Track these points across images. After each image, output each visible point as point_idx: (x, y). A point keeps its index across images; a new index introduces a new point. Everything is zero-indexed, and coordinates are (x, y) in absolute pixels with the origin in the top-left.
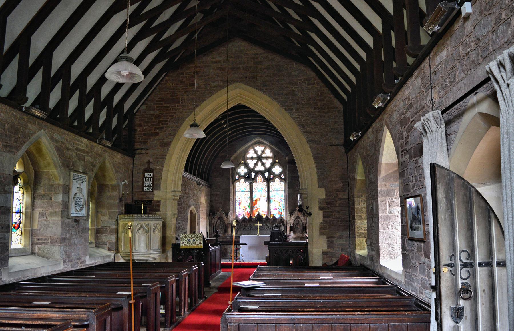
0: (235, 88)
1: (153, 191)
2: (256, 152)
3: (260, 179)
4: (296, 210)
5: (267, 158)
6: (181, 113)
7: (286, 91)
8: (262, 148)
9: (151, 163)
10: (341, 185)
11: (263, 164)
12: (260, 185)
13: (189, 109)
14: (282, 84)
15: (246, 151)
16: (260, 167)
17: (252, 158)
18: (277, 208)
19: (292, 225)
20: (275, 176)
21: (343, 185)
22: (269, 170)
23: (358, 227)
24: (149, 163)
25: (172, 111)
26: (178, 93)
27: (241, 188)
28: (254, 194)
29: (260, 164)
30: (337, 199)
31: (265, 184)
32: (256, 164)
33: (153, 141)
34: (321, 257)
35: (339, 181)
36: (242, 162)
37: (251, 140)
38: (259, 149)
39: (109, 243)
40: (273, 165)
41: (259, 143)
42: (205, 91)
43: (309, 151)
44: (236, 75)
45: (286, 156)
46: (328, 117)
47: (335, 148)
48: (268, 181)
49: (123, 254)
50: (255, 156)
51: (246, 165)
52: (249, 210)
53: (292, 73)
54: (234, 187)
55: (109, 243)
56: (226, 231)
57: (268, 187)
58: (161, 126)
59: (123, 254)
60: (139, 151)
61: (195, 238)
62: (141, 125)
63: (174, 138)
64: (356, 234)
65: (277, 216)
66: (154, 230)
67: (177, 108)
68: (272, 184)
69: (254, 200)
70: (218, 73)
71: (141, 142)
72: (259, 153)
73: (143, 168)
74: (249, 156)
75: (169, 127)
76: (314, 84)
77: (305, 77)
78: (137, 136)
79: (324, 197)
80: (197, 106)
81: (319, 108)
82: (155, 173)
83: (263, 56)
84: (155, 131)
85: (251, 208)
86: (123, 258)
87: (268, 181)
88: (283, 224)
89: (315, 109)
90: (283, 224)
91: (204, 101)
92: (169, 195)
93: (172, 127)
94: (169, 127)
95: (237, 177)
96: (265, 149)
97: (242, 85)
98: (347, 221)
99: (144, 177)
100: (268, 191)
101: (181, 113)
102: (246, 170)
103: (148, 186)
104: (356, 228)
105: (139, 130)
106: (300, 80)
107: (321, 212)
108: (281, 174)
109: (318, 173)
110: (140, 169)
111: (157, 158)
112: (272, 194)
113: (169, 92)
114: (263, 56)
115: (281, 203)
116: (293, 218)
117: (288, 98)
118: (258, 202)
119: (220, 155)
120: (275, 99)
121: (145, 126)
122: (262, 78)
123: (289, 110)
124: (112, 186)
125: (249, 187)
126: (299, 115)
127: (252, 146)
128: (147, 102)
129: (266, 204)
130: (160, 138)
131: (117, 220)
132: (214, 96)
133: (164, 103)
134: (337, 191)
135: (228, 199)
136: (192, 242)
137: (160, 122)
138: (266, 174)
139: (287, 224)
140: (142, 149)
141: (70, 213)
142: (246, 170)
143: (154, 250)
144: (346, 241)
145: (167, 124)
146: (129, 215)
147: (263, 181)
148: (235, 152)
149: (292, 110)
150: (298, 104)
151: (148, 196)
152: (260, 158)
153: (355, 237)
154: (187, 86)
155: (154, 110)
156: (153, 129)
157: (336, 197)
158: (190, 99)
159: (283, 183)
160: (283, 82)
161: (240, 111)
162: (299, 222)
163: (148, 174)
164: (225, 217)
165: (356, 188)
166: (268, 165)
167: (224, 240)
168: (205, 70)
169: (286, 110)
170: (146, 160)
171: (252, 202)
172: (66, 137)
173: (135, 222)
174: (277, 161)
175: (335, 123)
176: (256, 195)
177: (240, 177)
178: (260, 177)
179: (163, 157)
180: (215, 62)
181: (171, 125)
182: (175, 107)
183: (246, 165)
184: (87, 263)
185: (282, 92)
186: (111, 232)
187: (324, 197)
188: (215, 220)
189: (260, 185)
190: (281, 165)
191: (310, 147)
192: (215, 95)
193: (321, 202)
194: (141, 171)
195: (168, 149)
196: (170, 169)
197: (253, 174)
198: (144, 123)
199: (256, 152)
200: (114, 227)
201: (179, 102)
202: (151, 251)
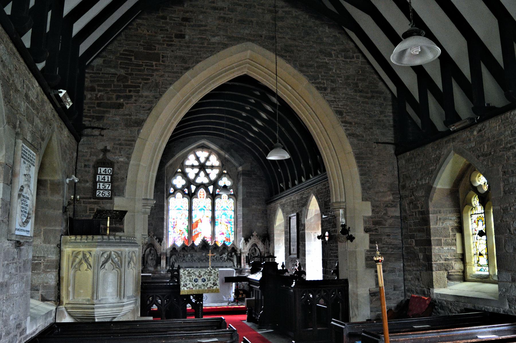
0: (246, 50)
1: (111, 198)
2: (198, 159)
3: (202, 194)
4: (253, 235)
5: (212, 167)
6: (162, 76)
7: (317, 62)
9: (109, 151)
10: (391, 198)
11: (207, 175)
12: (202, 201)
13: (174, 73)
14: (311, 52)
15: (185, 157)
16: (202, 179)
17: (193, 167)
18: (224, 232)
19: (247, 255)
21: (394, 198)
23: (435, 255)
24: (105, 151)
25: (146, 72)
26: (157, 46)
28: (194, 213)
29: (202, 174)
30: (386, 217)
31: (209, 201)
32: (197, 175)
33: (113, 116)
34: (369, 300)
35: (389, 193)
36: (179, 170)
37: (195, 141)
38: (202, 155)
39: (44, 287)
40: (220, 176)
41: (203, 147)
42: (201, 47)
43: (349, 148)
44: (247, 32)
45: (240, 165)
46: (372, 104)
47: (381, 146)
48: (213, 197)
49: (72, 308)
50: (196, 163)
51: (184, 175)
52: (186, 235)
53: (325, 39)
54: (168, 203)
55: (44, 287)
56: (158, 262)
57: (213, 205)
58: (128, 94)
59: (72, 308)
60: (89, 130)
61: (205, 277)
62: (93, 89)
63: (149, 114)
64: (434, 266)
66: (129, 263)
67: (155, 67)
68: (217, 201)
70: (219, 25)
71: (92, 117)
72: (202, 160)
73: (94, 158)
74: (187, 163)
75: (142, 96)
76: (353, 57)
77: (342, 47)
78: (86, 107)
79: (370, 214)
80: (187, 69)
81: (361, 91)
82: (116, 168)
83: (284, 9)
84: (118, 101)
85: (190, 232)
86: (70, 314)
87: (213, 197)
88: (236, 254)
89: (356, 91)
90: (236, 254)
91: (197, 62)
92: (139, 206)
93: (146, 97)
94: (142, 96)
95: (172, 190)
96: (209, 155)
97: (256, 47)
98: (399, 248)
99: (96, 174)
100: (213, 210)
101: (162, 76)
102: (183, 182)
103: (103, 189)
104: (433, 257)
105: (89, 96)
106: (335, 50)
107: (367, 235)
109: (361, 180)
110: (88, 160)
111: (120, 144)
112: (217, 214)
113: (141, 43)
114: (284, 9)
115: (229, 225)
116: (249, 246)
117: (321, 72)
118: (200, 224)
120: (301, 71)
121: (99, 91)
122: (283, 40)
123: (321, 89)
124: (53, 183)
125: (187, 205)
126: (335, 98)
127: (193, 151)
128: (104, 54)
129: (209, 227)
130: (126, 112)
131: (59, 246)
132: (212, 59)
133: (133, 58)
134: (387, 206)
135: (162, 220)
136: (200, 283)
137: (126, 87)
138: (211, 188)
139: (241, 254)
140: (93, 128)
141: (13, 229)
142: (183, 182)
143: (129, 298)
144: (399, 276)
145: (138, 92)
146: (84, 237)
147: (207, 197)
148: (173, 156)
149: (325, 89)
150: (332, 81)
151: (102, 206)
152: (202, 167)
153: (432, 270)
154: (172, 38)
155: (115, 67)
156: (114, 96)
157: (385, 214)
158: (176, 57)
159: (232, 201)
160: (313, 50)
161: (245, 84)
162: (256, 250)
163: (103, 169)
164: (157, 244)
165: (432, 200)
166: (213, 177)
167: (156, 275)
168: (201, 17)
169: (318, 88)
170: (100, 147)
171: (191, 225)
172: (15, 62)
173: (96, 250)
174: (225, 172)
175: (382, 113)
176: (197, 215)
177: (176, 190)
178: (202, 192)
179: (130, 143)
180: (215, 8)
181: (145, 94)
182: (152, 66)
183: (184, 175)
184: (28, 332)
185: (311, 63)
186: (47, 267)
187: (370, 214)
189: (202, 201)
191: (351, 144)
192: (215, 56)
193: (366, 220)
194: (92, 164)
195: (139, 131)
196: (141, 163)
197: (193, 188)
198: (98, 85)
199: (198, 159)
200: (53, 257)
201: (158, 60)
202: (125, 300)
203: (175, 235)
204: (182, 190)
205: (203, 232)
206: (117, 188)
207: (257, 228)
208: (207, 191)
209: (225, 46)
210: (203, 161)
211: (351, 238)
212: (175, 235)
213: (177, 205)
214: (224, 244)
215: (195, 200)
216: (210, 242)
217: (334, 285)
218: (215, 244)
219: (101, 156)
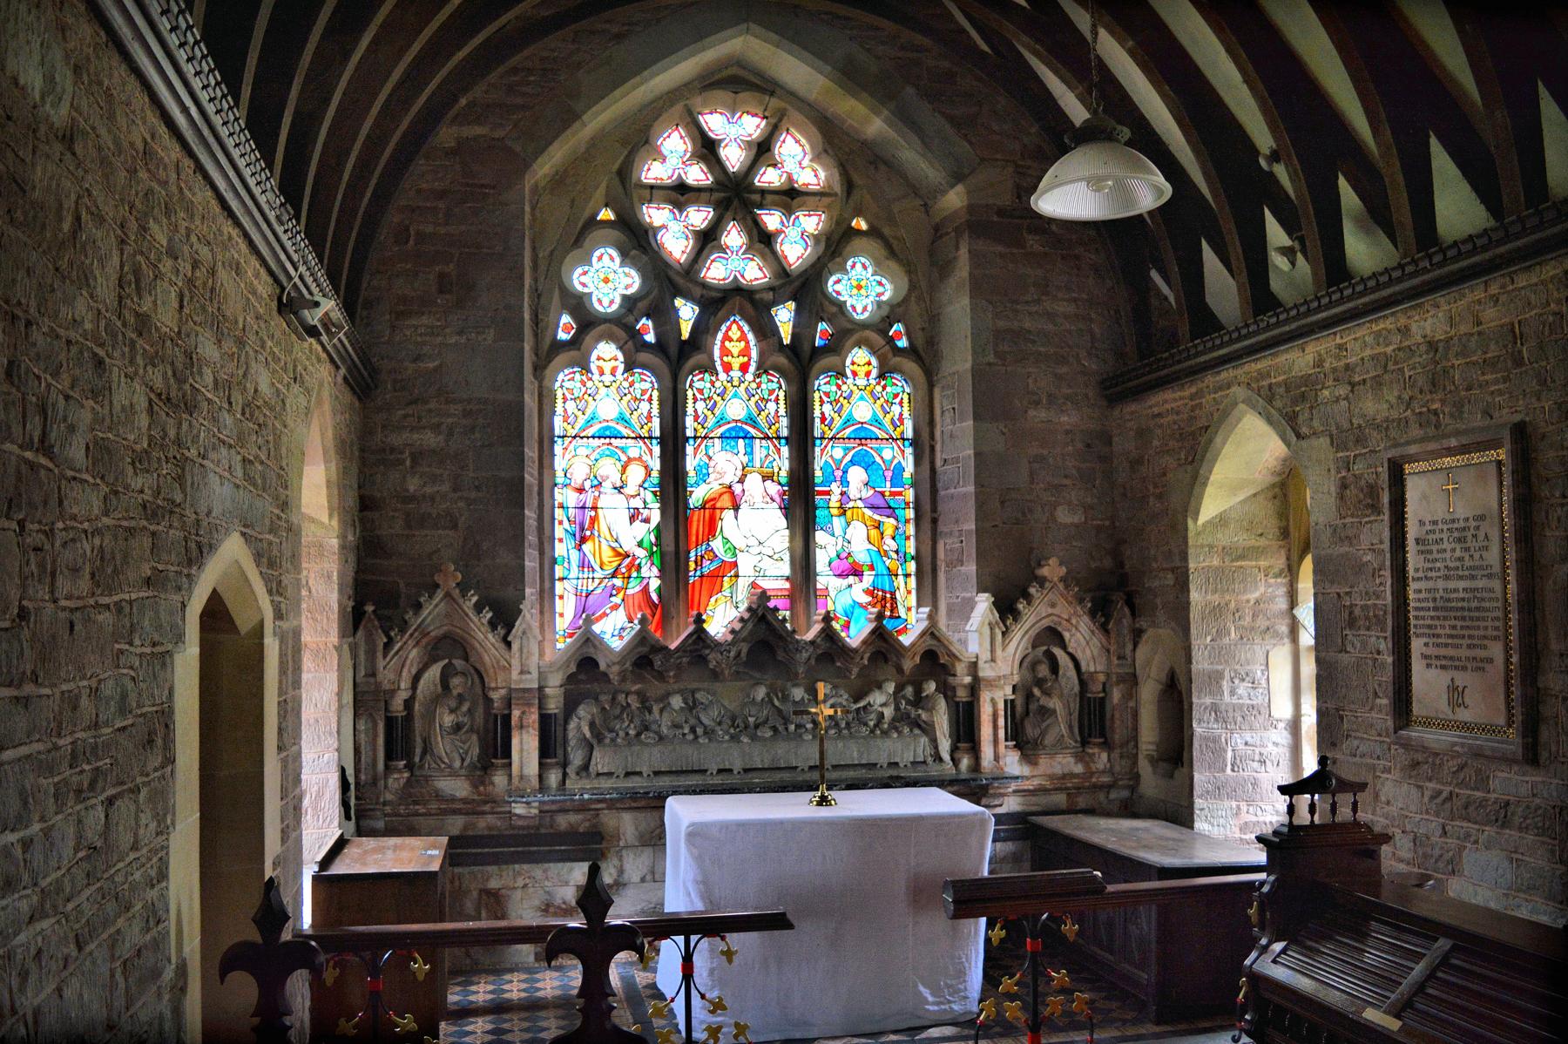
2: (707, 149)
8: (752, 126)
11: (763, 241)
15: (638, 138)
16: (735, 264)
20: (847, 332)
22: (806, 288)
27: (595, 424)
31: (774, 387)
32: (707, 240)
36: (606, 214)
40: (833, 247)
48: (799, 365)
51: (637, 242)
54: (546, 401)
56: (497, 748)
65: (857, 633)
69: (697, 496)
74: (655, 172)
87: (799, 365)
88: (946, 690)
90: (946, 690)
100: (801, 439)
108: (890, 314)
119: (446, 135)
127: (681, 106)
139: (974, 689)
148: (570, 118)
164: (485, 640)
171: (682, 522)
176: (713, 467)
177: (589, 323)
178: (735, 339)
183: (637, 242)
188: (405, 669)
189: (735, 392)
190: (891, 251)
197: (687, 312)
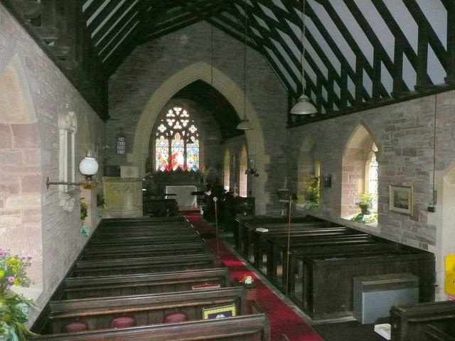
11: (181, 124)
12: (178, 141)
16: (178, 126)
40: (189, 125)
48: (184, 138)
51: (166, 124)
80: (166, 79)
102: (165, 128)
118: (176, 157)
138: (184, 133)
142: (165, 128)
152: (178, 118)
166: (185, 125)
171: (171, 157)
176: (174, 151)
178: (178, 135)
183: (166, 124)
197: (172, 132)
203: (160, 164)
204: (164, 134)
205: (179, 161)
206: (128, 149)
207: (211, 157)
208: (181, 134)
209: (188, 64)
210: (179, 115)
211: (258, 175)
212: (160, 164)
213: (161, 143)
214: (192, 170)
215: (173, 141)
216: (183, 169)
217: (251, 199)
218: (186, 170)
219: (119, 132)
